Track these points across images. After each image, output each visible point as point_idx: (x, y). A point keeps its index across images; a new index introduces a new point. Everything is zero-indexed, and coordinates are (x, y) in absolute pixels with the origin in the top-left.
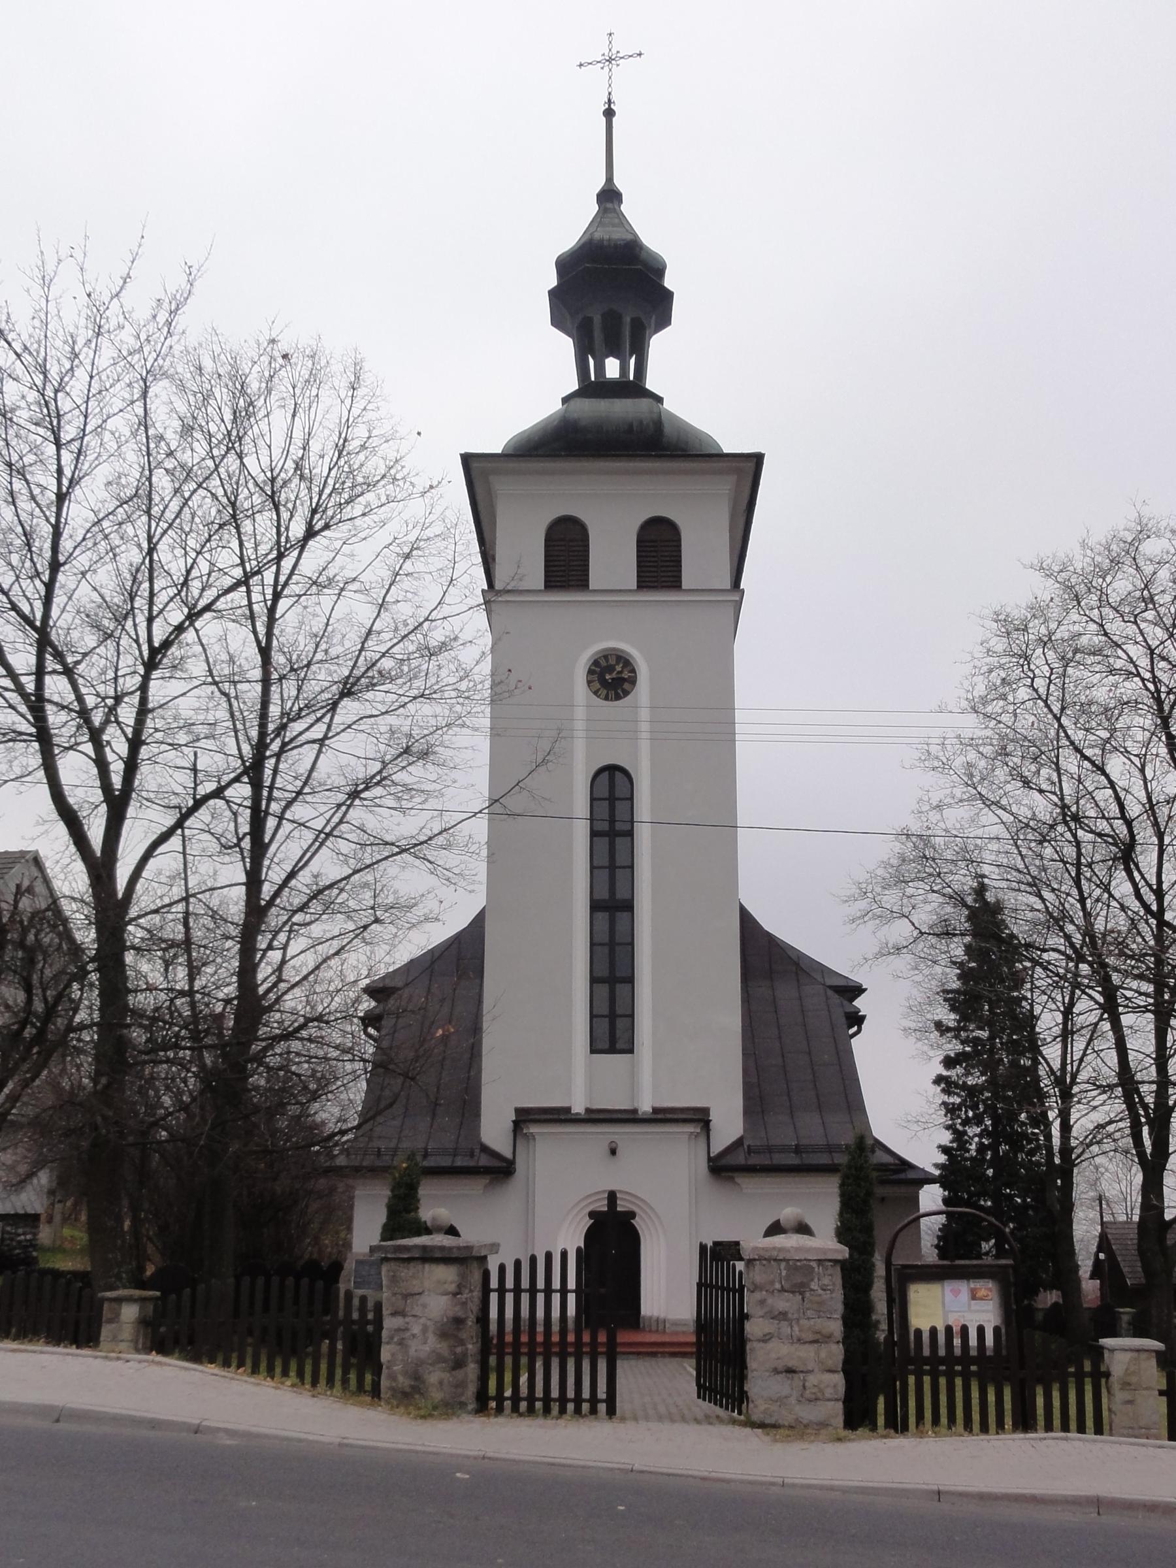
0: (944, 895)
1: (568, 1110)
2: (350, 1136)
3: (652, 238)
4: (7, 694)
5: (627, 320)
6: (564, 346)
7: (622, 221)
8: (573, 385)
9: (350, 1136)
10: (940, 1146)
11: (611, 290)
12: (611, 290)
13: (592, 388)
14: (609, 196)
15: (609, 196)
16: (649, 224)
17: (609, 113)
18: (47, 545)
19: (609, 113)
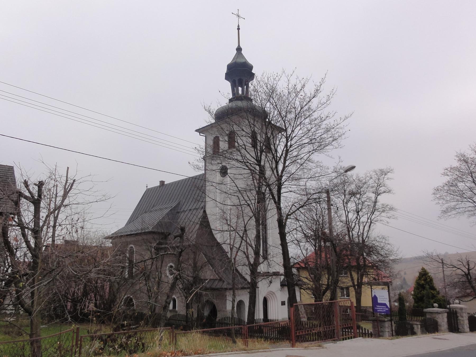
0: (327, 260)
1: (279, 272)
2: (331, 278)
3: (250, 60)
4: (250, 248)
5: (244, 81)
6: (228, 85)
7: (243, 57)
8: (231, 96)
9: (331, 278)
10: (196, 131)
11: (239, 73)
12: (239, 73)
13: (235, 97)
14: (239, 49)
15: (239, 49)
16: (249, 56)
17: (239, 29)
18: (280, 250)
19: (239, 29)
